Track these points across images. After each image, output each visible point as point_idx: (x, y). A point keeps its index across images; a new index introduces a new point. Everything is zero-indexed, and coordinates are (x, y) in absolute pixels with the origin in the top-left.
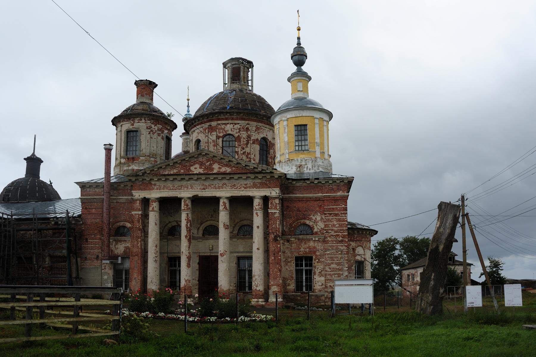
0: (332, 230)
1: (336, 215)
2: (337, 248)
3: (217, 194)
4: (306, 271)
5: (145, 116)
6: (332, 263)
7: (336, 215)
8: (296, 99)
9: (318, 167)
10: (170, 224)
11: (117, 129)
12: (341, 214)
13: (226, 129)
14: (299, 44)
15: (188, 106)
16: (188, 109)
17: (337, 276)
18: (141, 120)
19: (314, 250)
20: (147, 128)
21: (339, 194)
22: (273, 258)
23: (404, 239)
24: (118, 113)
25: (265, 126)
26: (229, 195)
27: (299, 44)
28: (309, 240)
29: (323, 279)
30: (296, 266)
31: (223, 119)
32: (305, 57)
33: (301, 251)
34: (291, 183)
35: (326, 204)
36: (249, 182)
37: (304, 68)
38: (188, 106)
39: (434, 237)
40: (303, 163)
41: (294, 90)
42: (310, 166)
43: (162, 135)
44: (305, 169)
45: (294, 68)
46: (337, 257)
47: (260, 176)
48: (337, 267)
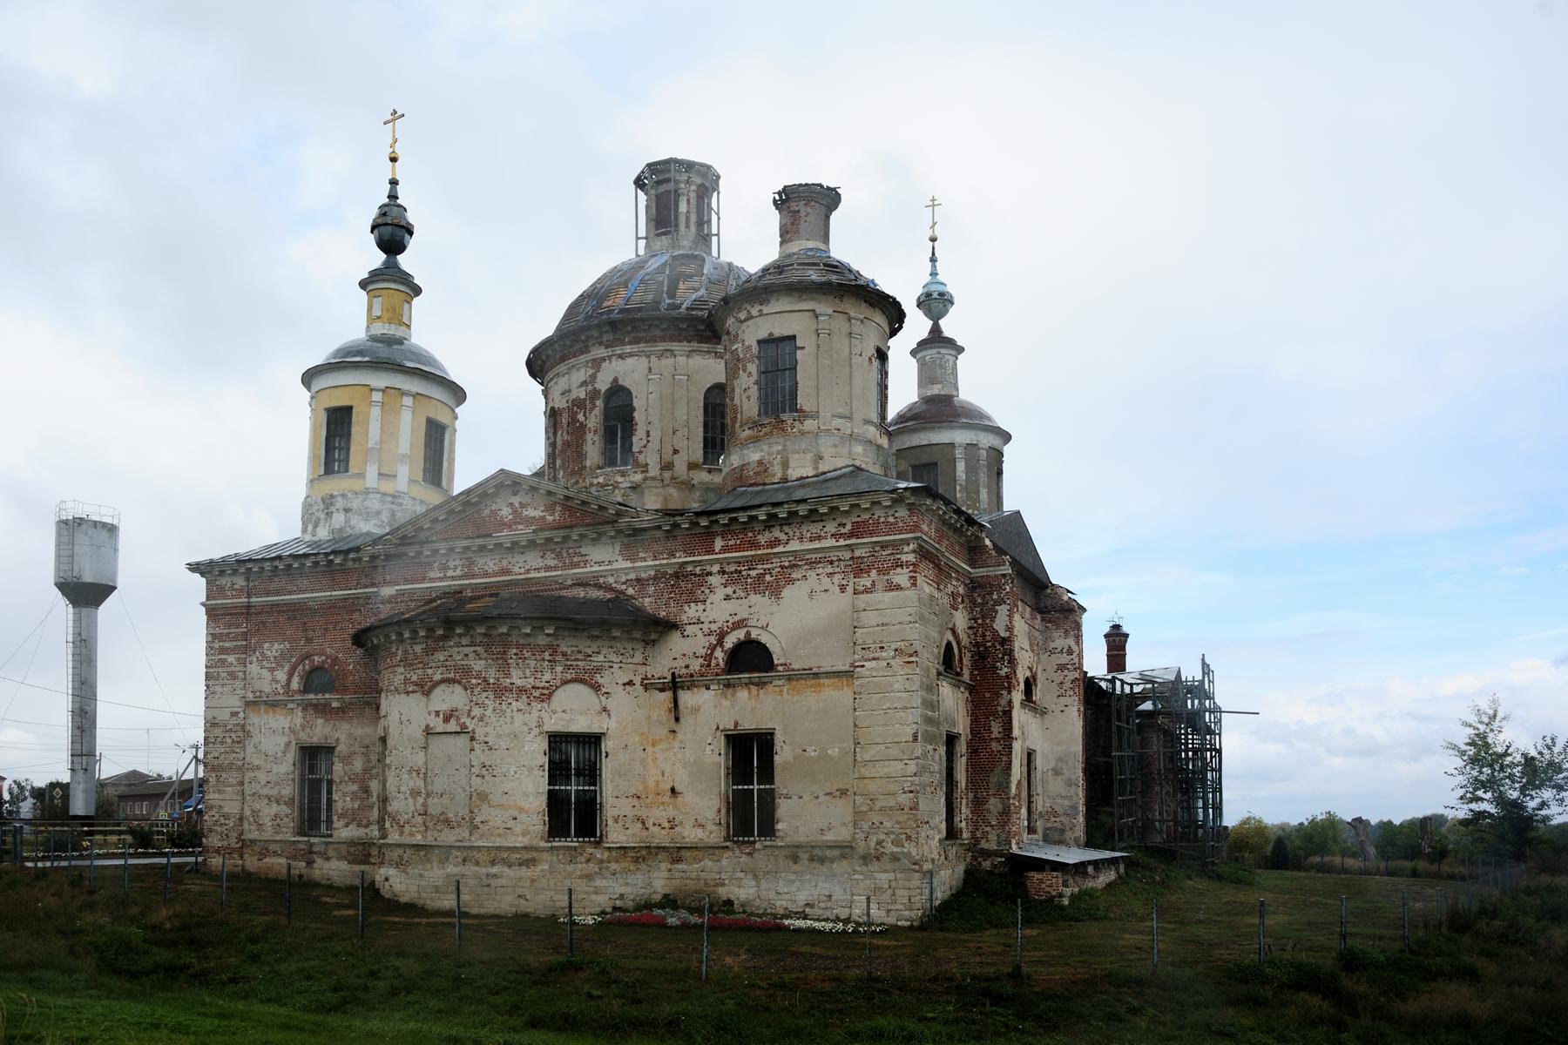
8: (373, 339)
11: (546, 393)
14: (393, 196)
15: (933, 260)
16: (934, 267)
22: (335, 704)
24: (547, 327)
27: (393, 196)
37: (403, 260)
38: (933, 260)
45: (378, 258)
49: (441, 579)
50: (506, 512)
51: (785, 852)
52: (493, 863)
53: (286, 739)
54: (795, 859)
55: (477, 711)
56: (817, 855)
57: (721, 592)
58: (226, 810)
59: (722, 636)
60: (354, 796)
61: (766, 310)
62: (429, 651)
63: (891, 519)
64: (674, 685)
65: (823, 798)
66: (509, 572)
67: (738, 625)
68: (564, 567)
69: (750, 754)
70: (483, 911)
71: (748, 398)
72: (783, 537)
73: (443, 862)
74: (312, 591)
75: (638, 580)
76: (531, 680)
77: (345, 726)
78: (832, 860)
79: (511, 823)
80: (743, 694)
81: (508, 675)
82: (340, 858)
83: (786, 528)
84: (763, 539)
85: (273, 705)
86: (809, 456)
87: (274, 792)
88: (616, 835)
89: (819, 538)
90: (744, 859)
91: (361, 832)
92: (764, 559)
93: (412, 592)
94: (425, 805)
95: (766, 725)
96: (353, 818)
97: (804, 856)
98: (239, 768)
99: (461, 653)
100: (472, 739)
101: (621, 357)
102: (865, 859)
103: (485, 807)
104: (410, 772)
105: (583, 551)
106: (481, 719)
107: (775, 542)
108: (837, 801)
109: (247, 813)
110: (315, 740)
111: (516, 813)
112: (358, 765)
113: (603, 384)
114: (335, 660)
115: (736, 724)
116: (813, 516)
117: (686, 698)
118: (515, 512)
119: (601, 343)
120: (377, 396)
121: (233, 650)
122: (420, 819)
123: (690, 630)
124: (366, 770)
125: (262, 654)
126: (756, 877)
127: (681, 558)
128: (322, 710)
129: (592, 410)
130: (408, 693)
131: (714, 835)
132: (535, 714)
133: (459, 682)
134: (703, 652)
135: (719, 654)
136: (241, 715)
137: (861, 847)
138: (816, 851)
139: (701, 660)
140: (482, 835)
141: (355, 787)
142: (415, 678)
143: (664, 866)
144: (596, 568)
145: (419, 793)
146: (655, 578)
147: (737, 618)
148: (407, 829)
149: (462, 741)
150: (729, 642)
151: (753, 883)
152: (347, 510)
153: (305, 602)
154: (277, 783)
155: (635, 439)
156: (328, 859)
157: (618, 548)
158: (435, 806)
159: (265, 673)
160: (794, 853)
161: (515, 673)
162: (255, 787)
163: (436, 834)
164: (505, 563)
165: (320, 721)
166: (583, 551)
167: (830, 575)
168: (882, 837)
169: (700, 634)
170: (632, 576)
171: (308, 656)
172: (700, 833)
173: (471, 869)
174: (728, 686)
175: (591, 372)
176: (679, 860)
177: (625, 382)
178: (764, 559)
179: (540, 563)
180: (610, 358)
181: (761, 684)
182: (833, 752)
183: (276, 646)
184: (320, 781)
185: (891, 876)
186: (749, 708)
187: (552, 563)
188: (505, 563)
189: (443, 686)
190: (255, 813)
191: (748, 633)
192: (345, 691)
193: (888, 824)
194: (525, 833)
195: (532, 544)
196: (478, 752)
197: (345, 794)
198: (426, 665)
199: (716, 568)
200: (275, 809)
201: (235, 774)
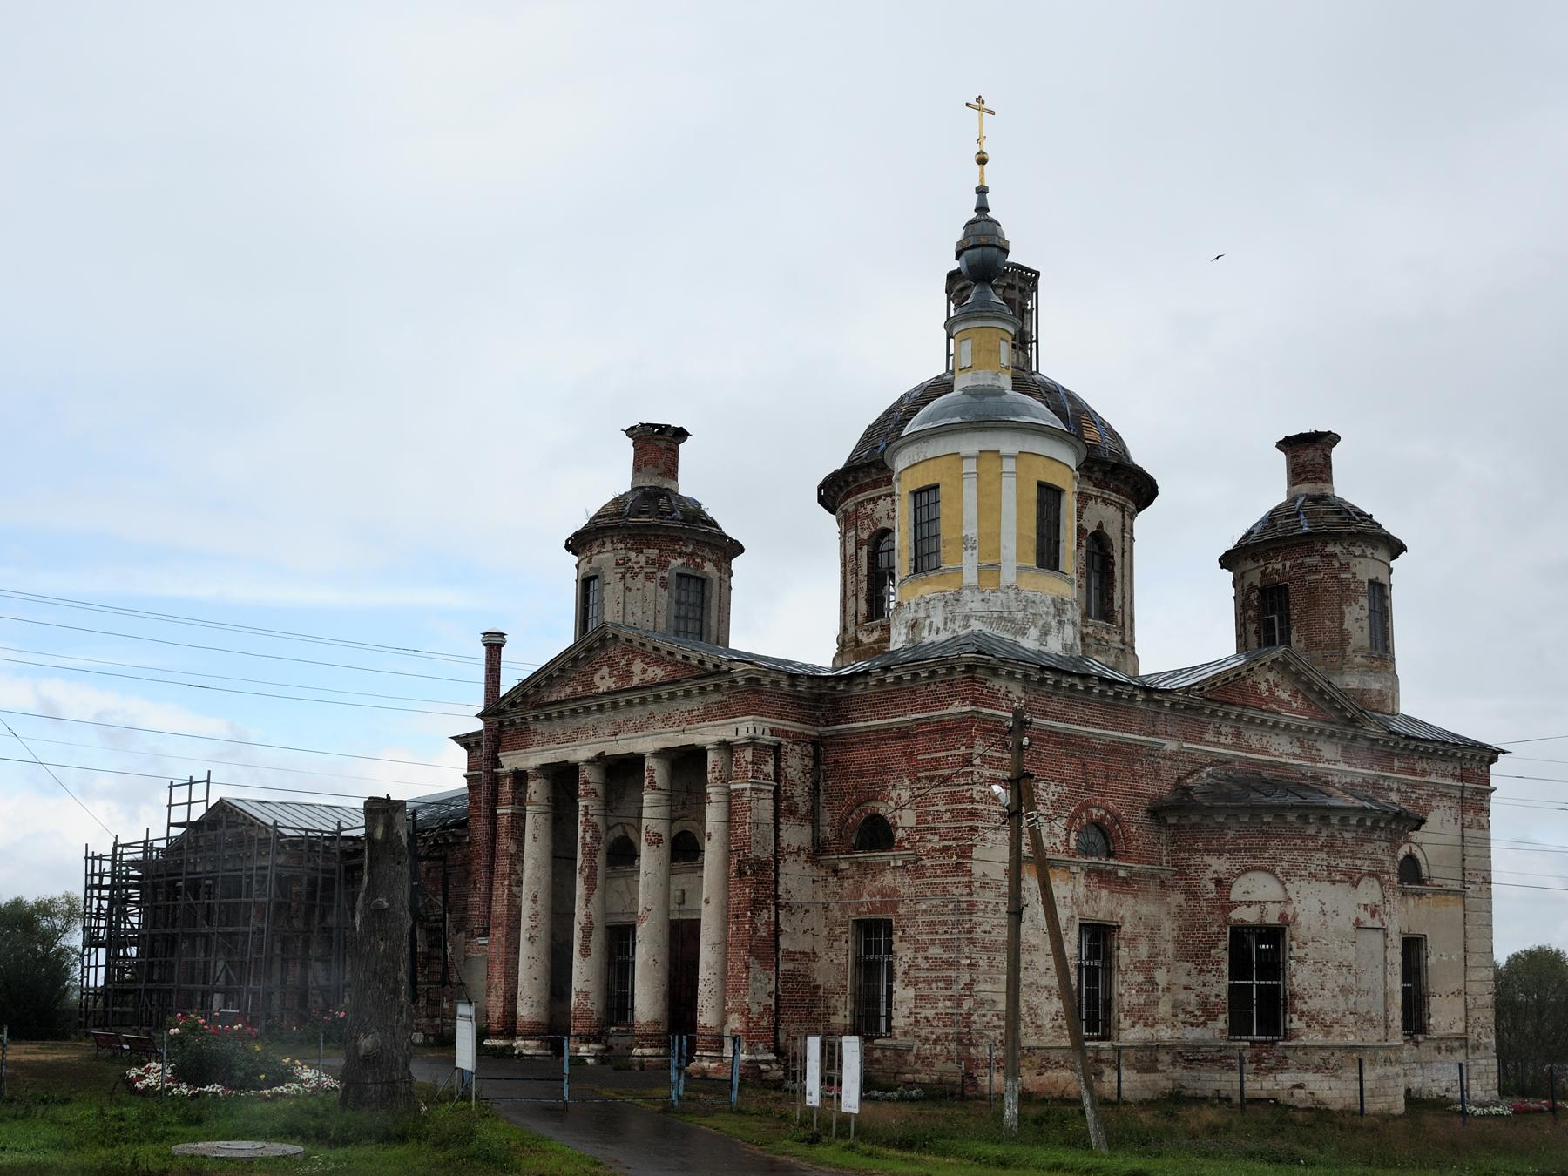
0: (934, 830)
1: (945, 780)
2: (945, 893)
3: (697, 739)
5: (609, 533)
6: (932, 943)
7: (945, 780)
9: (967, 618)
12: (958, 775)
13: (876, 516)
14: (982, 208)
17: (941, 984)
18: (603, 545)
19: (891, 899)
20: (617, 564)
21: (952, 709)
22: (1121, 873)
23: (38, 904)
26: (660, 744)
27: (982, 208)
28: (883, 867)
29: (911, 992)
31: (868, 487)
33: (862, 904)
34: (834, 688)
35: (921, 746)
36: (696, 704)
40: (922, 614)
42: (938, 620)
43: (659, 575)
44: (925, 633)
46: (944, 923)
47: (709, 683)
48: (945, 956)
62: (1360, 841)
74: (1095, 725)
77: (1130, 901)
96: (1141, 1016)
104: (1339, 967)
107: (1424, 773)
110: (1100, 916)
112: (1143, 950)
114: (1117, 819)
116: (1444, 757)
120: (1009, 465)
122: (1351, 1018)
130: (1334, 882)
144: (1326, 765)
145: (1351, 991)
148: (1336, 1029)
149: (1379, 936)
165: (1104, 892)
171: (1086, 807)
178: (1420, 785)
179: (1287, 748)
184: (878, 963)
187: (1298, 751)
192: (1127, 855)
197: (1130, 986)
198: (1354, 856)
199: (1395, 786)
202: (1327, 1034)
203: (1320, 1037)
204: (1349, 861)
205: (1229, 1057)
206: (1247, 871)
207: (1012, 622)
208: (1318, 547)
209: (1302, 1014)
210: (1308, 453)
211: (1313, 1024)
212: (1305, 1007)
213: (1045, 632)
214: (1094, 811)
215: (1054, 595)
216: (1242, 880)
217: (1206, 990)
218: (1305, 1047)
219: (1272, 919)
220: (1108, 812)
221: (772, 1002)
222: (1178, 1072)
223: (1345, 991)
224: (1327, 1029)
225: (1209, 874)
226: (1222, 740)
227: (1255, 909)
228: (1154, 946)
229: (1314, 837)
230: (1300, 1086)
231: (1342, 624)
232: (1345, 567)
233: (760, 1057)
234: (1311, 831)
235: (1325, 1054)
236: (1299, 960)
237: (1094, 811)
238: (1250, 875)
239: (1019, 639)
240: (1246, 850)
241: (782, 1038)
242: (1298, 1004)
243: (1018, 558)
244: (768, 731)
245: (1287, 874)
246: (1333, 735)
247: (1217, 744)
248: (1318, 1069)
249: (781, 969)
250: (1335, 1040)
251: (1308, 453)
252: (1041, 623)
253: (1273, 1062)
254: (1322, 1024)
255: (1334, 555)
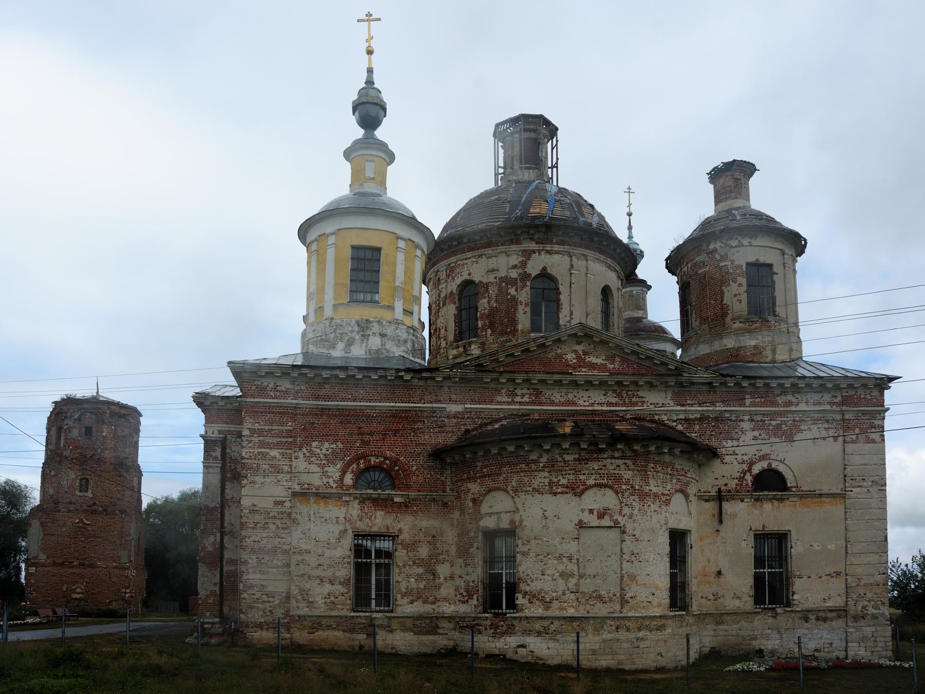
4: (377, 565)
10: (778, 463)
14: (370, 82)
16: (630, 232)
22: (397, 500)
25: (463, 256)
27: (370, 82)
30: (355, 557)
32: (382, 113)
37: (380, 133)
39: (204, 484)
41: (357, 176)
45: (360, 133)
49: (509, 403)
50: (570, 357)
51: (798, 615)
52: (640, 629)
53: (341, 528)
54: (807, 620)
55: (626, 511)
56: (822, 616)
57: (750, 435)
58: (270, 589)
59: (751, 464)
60: (419, 577)
61: (754, 243)
63: (868, 397)
64: (720, 497)
65: (824, 578)
66: (574, 404)
67: (763, 458)
68: (624, 404)
69: (772, 549)
70: (634, 667)
71: (740, 301)
72: (794, 400)
73: (597, 631)
75: (686, 420)
76: (661, 488)
78: (832, 620)
79: (651, 598)
80: (768, 506)
81: (648, 484)
82: (405, 629)
83: (797, 396)
84: (781, 400)
85: (322, 496)
86: (787, 347)
87: (329, 573)
88: (695, 608)
89: (819, 404)
90: (770, 620)
91: (428, 608)
92: (780, 414)
93: (478, 412)
94: (577, 585)
95: (784, 528)
96: (416, 596)
97: (812, 617)
98: (286, 552)
99: (613, 465)
100: (624, 532)
101: (548, 252)
102: (855, 618)
103: (633, 585)
105: (641, 393)
106: (630, 517)
107: (789, 404)
108: (834, 580)
109: (295, 591)
111: (654, 590)
113: (533, 268)
114: (396, 462)
115: (764, 526)
117: (728, 507)
118: (579, 357)
119: (532, 239)
121: (277, 446)
123: (727, 459)
124: (431, 556)
125: (310, 451)
126: (779, 632)
127: (720, 407)
128: (378, 503)
129: (522, 288)
130: (555, 494)
131: (748, 604)
132: (664, 514)
133: (611, 487)
134: (738, 475)
135: (749, 478)
136: (288, 504)
137: (852, 610)
138: (821, 614)
139: (736, 481)
140: (632, 607)
141: (421, 570)
142: (564, 481)
143: (710, 627)
145: (572, 575)
146: (700, 419)
147: (762, 453)
149: (614, 534)
150: (756, 469)
151: (778, 636)
152: (383, 335)
153: (362, 409)
154: (329, 566)
155: (561, 315)
156: (391, 631)
157: (670, 395)
158: (587, 586)
159: (314, 468)
160: (805, 616)
161: (652, 482)
162: (303, 569)
163: (588, 608)
164: (570, 396)
165: (380, 513)
166: (641, 393)
167: (826, 429)
168: (866, 603)
169: (735, 462)
170: (682, 417)
171: (364, 456)
172: (737, 603)
173: (623, 635)
174: (757, 500)
175: (521, 259)
176: (721, 623)
177: (553, 272)
178: (780, 414)
180: (539, 251)
181: (781, 500)
182: (831, 547)
183: (326, 445)
185: (873, 629)
186: (771, 515)
187: (614, 400)
188: (570, 396)
189: (595, 490)
190: (304, 593)
191: (770, 464)
192: (408, 487)
193: (869, 595)
194: (659, 605)
195: (603, 384)
196: (628, 542)
198: (577, 472)
199: (746, 418)
200: (328, 588)
201: (280, 557)
202: (547, 608)
203: (540, 610)
204: (571, 477)
205: (480, 625)
206: (489, 491)
207: (327, 341)
208: (704, 248)
209: (526, 593)
210: (732, 177)
211: (535, 600)
212: (527, 589)
213: (350, 343)
214: (373, 459)
215: (358, 318)
216: (488, 498)
217: (468, 578)
218: (527, 618)
219: (505, 525)
220: (386, 458)
221: (217, 589)
222: (456, 635)
223: (565, 576)
224: (547, 605)
225: (470, 496)
226: (518, 399)
227: (494, 518)
228: (435, 548)
229: (536, 462)
230: (523, 646)
231: (722, 301)
232: (724, 257)
233: (206, 620)
234: (534, 456)
235: (546, 623)
236: (524, 554)
237: (373, 459)
238: (492, 494)
239: (331, 351)
240: (489, 475)
241: (226, 610)
242: (523, 586)
243: (335, 299)
244: (216, 432)
245: (516, 491)
246: (463, 380)
247: (513, 402)
248: (539, 634)
249: (225, 569)
250: (554, 612)
251: (732, 177)
252: (347, 338)
253: (505, 628)
254: (542, 600)
255: (715, 250)
